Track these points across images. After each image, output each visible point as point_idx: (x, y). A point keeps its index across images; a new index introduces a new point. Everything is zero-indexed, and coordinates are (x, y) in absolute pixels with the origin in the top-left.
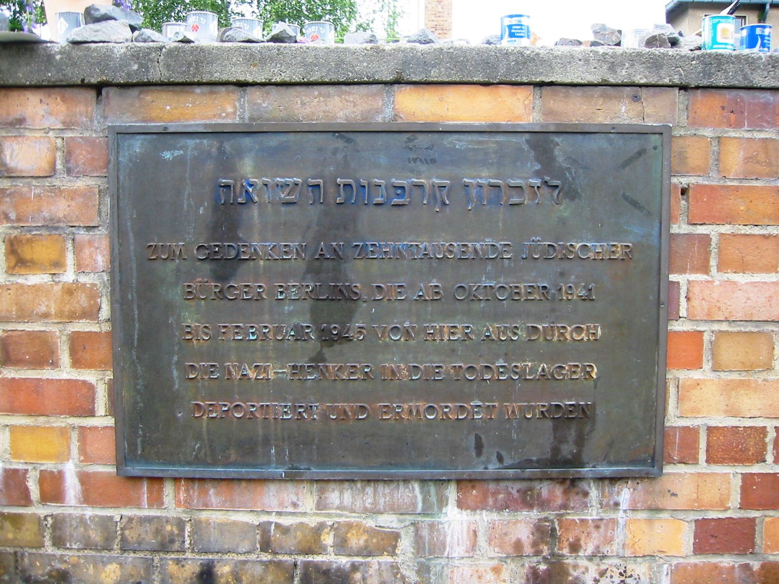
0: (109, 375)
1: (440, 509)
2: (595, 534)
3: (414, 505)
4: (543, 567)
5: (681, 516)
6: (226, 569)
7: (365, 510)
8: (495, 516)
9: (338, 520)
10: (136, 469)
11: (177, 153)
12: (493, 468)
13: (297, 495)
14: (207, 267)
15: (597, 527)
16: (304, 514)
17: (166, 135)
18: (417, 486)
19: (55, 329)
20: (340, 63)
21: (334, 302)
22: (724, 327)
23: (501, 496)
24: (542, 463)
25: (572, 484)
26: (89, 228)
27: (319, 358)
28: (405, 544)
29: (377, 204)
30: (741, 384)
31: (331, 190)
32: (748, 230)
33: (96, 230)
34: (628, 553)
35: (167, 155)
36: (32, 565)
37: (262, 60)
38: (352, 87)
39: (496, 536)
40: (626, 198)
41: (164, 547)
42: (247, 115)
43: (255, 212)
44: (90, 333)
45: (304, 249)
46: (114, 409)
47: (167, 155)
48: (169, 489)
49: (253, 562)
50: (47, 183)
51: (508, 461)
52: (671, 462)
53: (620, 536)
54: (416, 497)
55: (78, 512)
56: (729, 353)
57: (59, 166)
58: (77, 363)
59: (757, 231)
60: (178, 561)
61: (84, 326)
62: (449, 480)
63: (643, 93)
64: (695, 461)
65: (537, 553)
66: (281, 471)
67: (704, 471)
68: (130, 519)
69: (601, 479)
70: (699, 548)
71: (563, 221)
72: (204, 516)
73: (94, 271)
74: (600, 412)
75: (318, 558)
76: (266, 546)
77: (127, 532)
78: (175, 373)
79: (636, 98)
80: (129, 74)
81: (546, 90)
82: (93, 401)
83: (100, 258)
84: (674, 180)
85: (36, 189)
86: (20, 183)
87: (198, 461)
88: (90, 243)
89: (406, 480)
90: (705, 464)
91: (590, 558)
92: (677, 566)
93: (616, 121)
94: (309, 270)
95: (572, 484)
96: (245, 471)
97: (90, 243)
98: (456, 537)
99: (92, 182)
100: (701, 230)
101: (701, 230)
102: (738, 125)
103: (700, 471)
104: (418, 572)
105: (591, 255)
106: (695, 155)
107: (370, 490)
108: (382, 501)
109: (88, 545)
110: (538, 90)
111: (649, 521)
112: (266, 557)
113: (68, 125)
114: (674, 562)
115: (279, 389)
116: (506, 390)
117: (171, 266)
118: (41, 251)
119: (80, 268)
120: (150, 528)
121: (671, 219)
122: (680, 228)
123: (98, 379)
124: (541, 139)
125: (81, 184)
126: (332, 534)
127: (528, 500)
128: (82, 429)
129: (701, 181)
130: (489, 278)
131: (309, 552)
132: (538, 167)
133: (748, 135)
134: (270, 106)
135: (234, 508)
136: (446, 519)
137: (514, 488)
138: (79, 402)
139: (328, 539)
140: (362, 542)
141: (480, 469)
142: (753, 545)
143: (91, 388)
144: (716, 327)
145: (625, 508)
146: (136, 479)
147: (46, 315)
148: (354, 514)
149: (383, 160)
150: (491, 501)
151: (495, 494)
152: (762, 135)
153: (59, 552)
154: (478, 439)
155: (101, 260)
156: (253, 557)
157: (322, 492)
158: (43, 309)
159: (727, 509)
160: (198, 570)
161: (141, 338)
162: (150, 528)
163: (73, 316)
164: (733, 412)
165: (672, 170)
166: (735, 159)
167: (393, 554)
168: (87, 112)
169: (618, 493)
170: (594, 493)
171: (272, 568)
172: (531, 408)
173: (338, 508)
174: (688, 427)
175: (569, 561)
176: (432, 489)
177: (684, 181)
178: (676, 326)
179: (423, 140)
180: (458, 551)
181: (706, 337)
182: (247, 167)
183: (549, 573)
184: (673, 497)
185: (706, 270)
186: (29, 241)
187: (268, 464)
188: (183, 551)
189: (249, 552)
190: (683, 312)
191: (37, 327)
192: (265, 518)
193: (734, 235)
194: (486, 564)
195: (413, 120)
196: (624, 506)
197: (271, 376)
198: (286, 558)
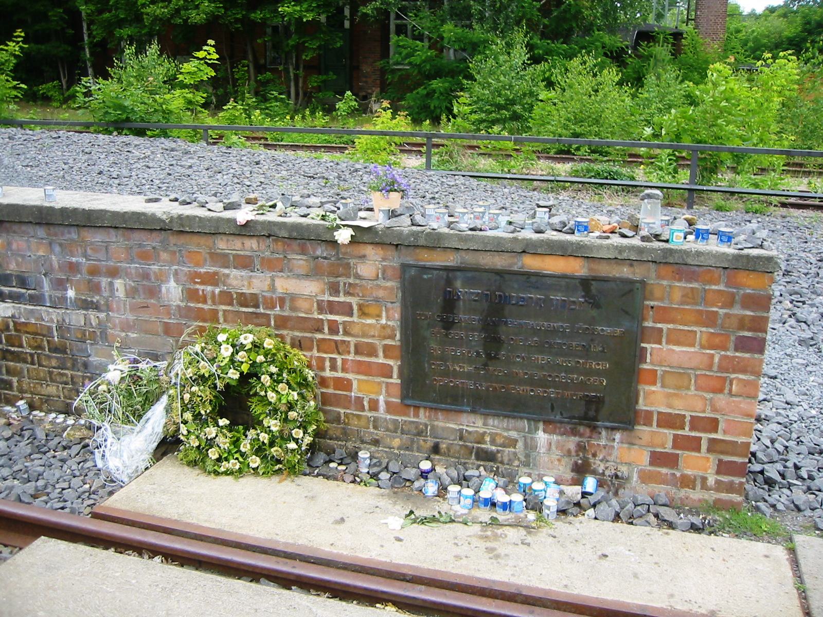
0: (399, 363)
2: (603, 450)
3: (524, 429)
4: (580, 462)
6: (444, 446)
7: (504, 428)
8: (559, 438)
10: (409, 402)
11: (429, 276)
12: (558, 417)
14: (441, 324)
15: (605, 448)
17: (425, 269)
19: (377, 342)
20: (499, 243)
21: (493, 342)
22: (668, 369)
24: (579, 418)
25: (594, 428)
26: (392, 303)
27: (486, 365)
28: (520, 445)
30: (675, 395)
31: (493, 297)
32: (681, 327)
34: (618, 461)
35: (425, 277)
36: (364, 435)
37: (466, 239)
39: (560, 446)
40: (622, 309)
41: (419, 434)
42: (459, 262)
43: (461, 303)
45: (481, 320)
46: (401, 376)
47: (425, 277)
48: (422, 411)
49: (456, 444)
50: (375, 283)
51: (565, 416)
52: (639, 424)
53: (615, 453)
55: (383, 416)
56: (669, 380)
57: (380, 276)
58: (386, 356)
59: (686, 328)
60: (424, 441)
61: (389, 342)
63: (635, 263)
64: (651, 425)
65: (578, 455)
66: (469, 409)
68: (405, 421)
69: (607, 428)
70: (652, 463)
71: (593, 318)
72: (436, 423)
73: (394, 320)
74: (607, 399)
75: (483, 446)
76: (461, 438)
78: (426, 365)
79: (631, 265)
80: (410, 242)
84: (647, 303)
85: (370, 285)
86: (364, 282)
87: (434, 401)
89: (521, 418)
91: (601, 461)
92: (641, 470)
94: (483, 329)
95: (594, 428)
100: (659, 325)
101: (659, 325)
102: (680, 280)
104: (525, 457)
105: (605, 333)
106: (657, 293)
107: (506, 420)
109: (388, 430)
111: (629, 449)
112: (461, 443)
113: (384, 259)
114: (640, 468)
115: (468, 376)
116: (565, 386)
117: (426, 322)
118: (372, 310)
119: (388, 318)
120: (413, 426)
121: (644, 319)
122: (649, 324)
123: (394, 364)
124: (585, 283)
125: (389, 284)
127: (574, 433)
128: (387, 383)
130: (560, 339)
131: (479, 443)
132: (583, 294)
133: (684, 285)
134: (470, 259)
135: (449, 421)
137: (568, 427)
138: (386, 372)
139: (488, 439)
140: (501, 441)
141: (553, 418)
142: (677, 465)
143: (391, 367)
144: (663, 368)
146: (409, 406)
147: (374, 336)
149: (516, 286)
150: (558, 431)
151: (560, 428)
152: (691, 286)
153: (376, 432)
154: (552, 405)
155: (397, 316)
156: (456, 442)
157: (485, 419)
158: (372, 333)
159: (665, 448)
160: (432, 445)
161: (413, 348)
162: (413, 426)
163: (385, 338)
164: (670, 406)
165: (328, 460)
166: (677, 295)
167: (515, 448)
170: (604, 433)
171: (463, 447)
172: (576, 395)
175: (592, 461)
176: (532, 423)
177: (652, 303)
178: (645, 366)
179: (533, 279)
180: (543, 450)
181: (659, 373)
182: (458, 284)
183: (582, 464)
185: (660, 343)
186: (367, 306)
187: (463, 405)
188: (426, 436)
189: (454, 440)
190: (648, 360)
191: (370, 341)
192: (461, 427)
193: (674, 329)
194: (554, 457)
196: (617, 441)
197: (466, 370)
198: (469, 444)
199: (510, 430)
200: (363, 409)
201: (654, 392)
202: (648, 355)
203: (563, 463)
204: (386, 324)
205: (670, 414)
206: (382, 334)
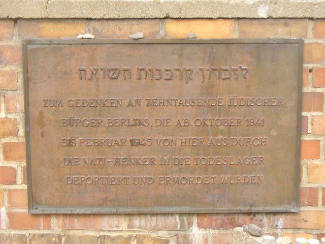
1: (189, 228)
3: (176, 226)
5: (310, 231)
8: (216, 231)
9: (139, 234)
13: (118, 221)
16: (122, 231)
18: (177, 217)
23: (219, 222)
29: (157, 79)
33: (16, 91)
38: (283, 16)
44: (14, 143)
54: (177, 222)
62: (193, 214)
64: (317, 205)
67: (321, 209)
68: (34, 235)
72: (71, 233)
73: (15, 112)
77: (32, 242)
79: (286, 25)
81: (241, 22)
82: (15, 177)
83: (18, 106)
88: (13, 97)
89: (172, 214)
90: (321, 206)
93: (276, 36)
96: (222, 207)
97: (13, 97)
98: (197, 242)
99: (13, 68)
100: (319, 90)
101: (319, 90)
103: (319, 209)
107: (154, 218)
108: (160, 224)
110: (237, 22)
126: (136, 240)
128: (10, 191)
129: (319, 66)
136: (192, 233)
143: (14, 170)
145: (281, 228)
148: (146, 231)
151: (216, 220)
168: (10, 32)
169: (278, 220)
173: (138, 228)
174: (312, 188)
177: (310, 66)
184: (306, 223)
190: (309, 131)
195: (174, 37)
196: (280, 226)
201: (317, 166)
202: (309, 125)
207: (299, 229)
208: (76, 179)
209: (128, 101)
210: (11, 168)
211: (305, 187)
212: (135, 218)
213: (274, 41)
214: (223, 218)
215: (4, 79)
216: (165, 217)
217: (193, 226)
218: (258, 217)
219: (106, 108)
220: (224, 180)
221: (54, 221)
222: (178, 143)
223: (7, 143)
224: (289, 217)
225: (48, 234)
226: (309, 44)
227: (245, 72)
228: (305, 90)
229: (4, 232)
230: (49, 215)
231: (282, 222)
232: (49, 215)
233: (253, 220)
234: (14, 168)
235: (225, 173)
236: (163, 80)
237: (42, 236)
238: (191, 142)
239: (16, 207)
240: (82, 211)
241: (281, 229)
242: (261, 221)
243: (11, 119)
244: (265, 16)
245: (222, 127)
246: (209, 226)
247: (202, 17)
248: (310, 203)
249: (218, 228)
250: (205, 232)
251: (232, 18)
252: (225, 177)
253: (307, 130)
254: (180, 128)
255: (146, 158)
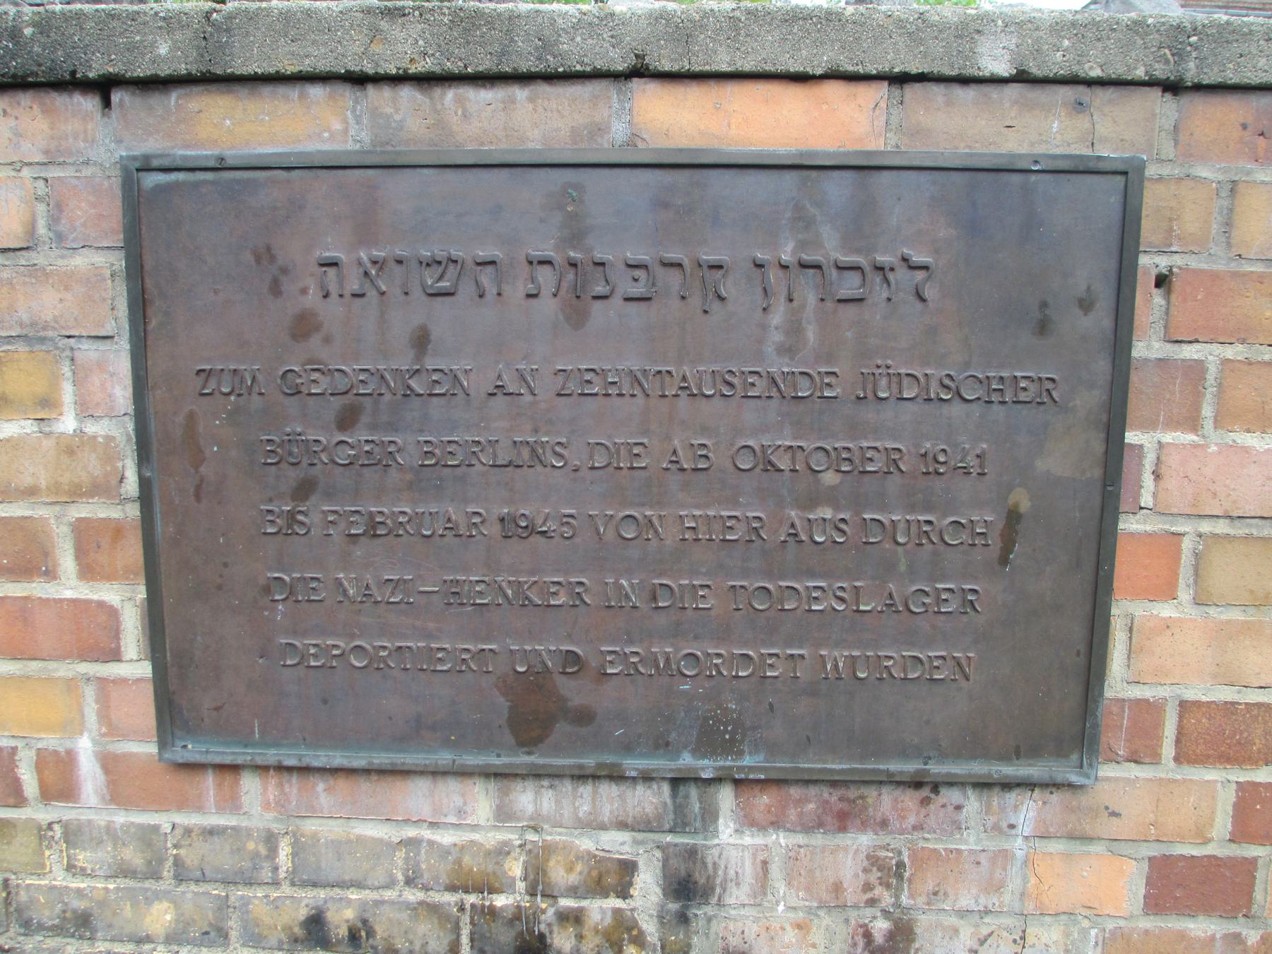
1: (705, 829)
8: (800, 839)
10: (192, 750)
13: (463, 795)
16: (475, 827)
22: (1222, 527)
34: (1030, 907)
56: (1227, 572)
57: (42, 230)
58: (88, 571)
64: (1155, 759)
67: (1170, 776)
68: (188, 831)
70: (1155, 903)
72: (310, 826)
90: (1172, 764)
103: (1163, 775)
107: (586, 790)
112: (413, 896)
114: (1110, 925)
119: (85, 411)
123: (125, 600)
125: (80, 261)
128: (102, 682)
136: (716, 841)
143: (112, 613)
144: (1206, 527)
151: (801, 802)
156: (389, 894)
159: (1206, 841)
163: (76, 493)
167: (624, 894)
185: (1193, 423)
189: (387, 887)
190: (1146, 499)
193: (1248, 362)
199: (603, 827)
200: (19, 800)
201: (1167, 625)
202: (1148, 480)
203: (817, 936)
204: (80, 433)
205: (1230, 706)
206: (66, 479)
207: (1086, 839)
208: (312, 651)
209: (493, 375)
210: (101, 604)
211: (1120, 696)
212: (518, 785)
213: (1036, 162)
214: (826, 795)
215: (69, 296)
216: (623, 788)
217: (721, 821)
218: (951, 796)
219: (416, 402)
220: (836, 666)
221: (250, 784)
222: (671, 535)
223: (85, 519)
224: (1055, 798)
225: (233, 828)
226: (1161, 179)
227: (920, 275)
228: (1140, 350)
229: (92, 816)
230: (234, 768)
231: (1031, 814)
232: (234, 768)
233: (932, 806)
234: (112, 607)
235: (837, 645)
236: (621, 302)
237: (211, 832)
238: (717, 526)
239: (125, 737)
240: (339, 759)
241: (1026, 838)
242: (958, 808)
243: (95, 437)
244: (1003, 68)
245: (830, 478)
246: (777, 824)
247: (769, 68)
248: (1136, 752)
249: (807, 829)
250: (759, 840)
251: (879, 77)
252: (837, 656)
253: (1137, 496)
254: (680, 476)
255: (559, 583)
